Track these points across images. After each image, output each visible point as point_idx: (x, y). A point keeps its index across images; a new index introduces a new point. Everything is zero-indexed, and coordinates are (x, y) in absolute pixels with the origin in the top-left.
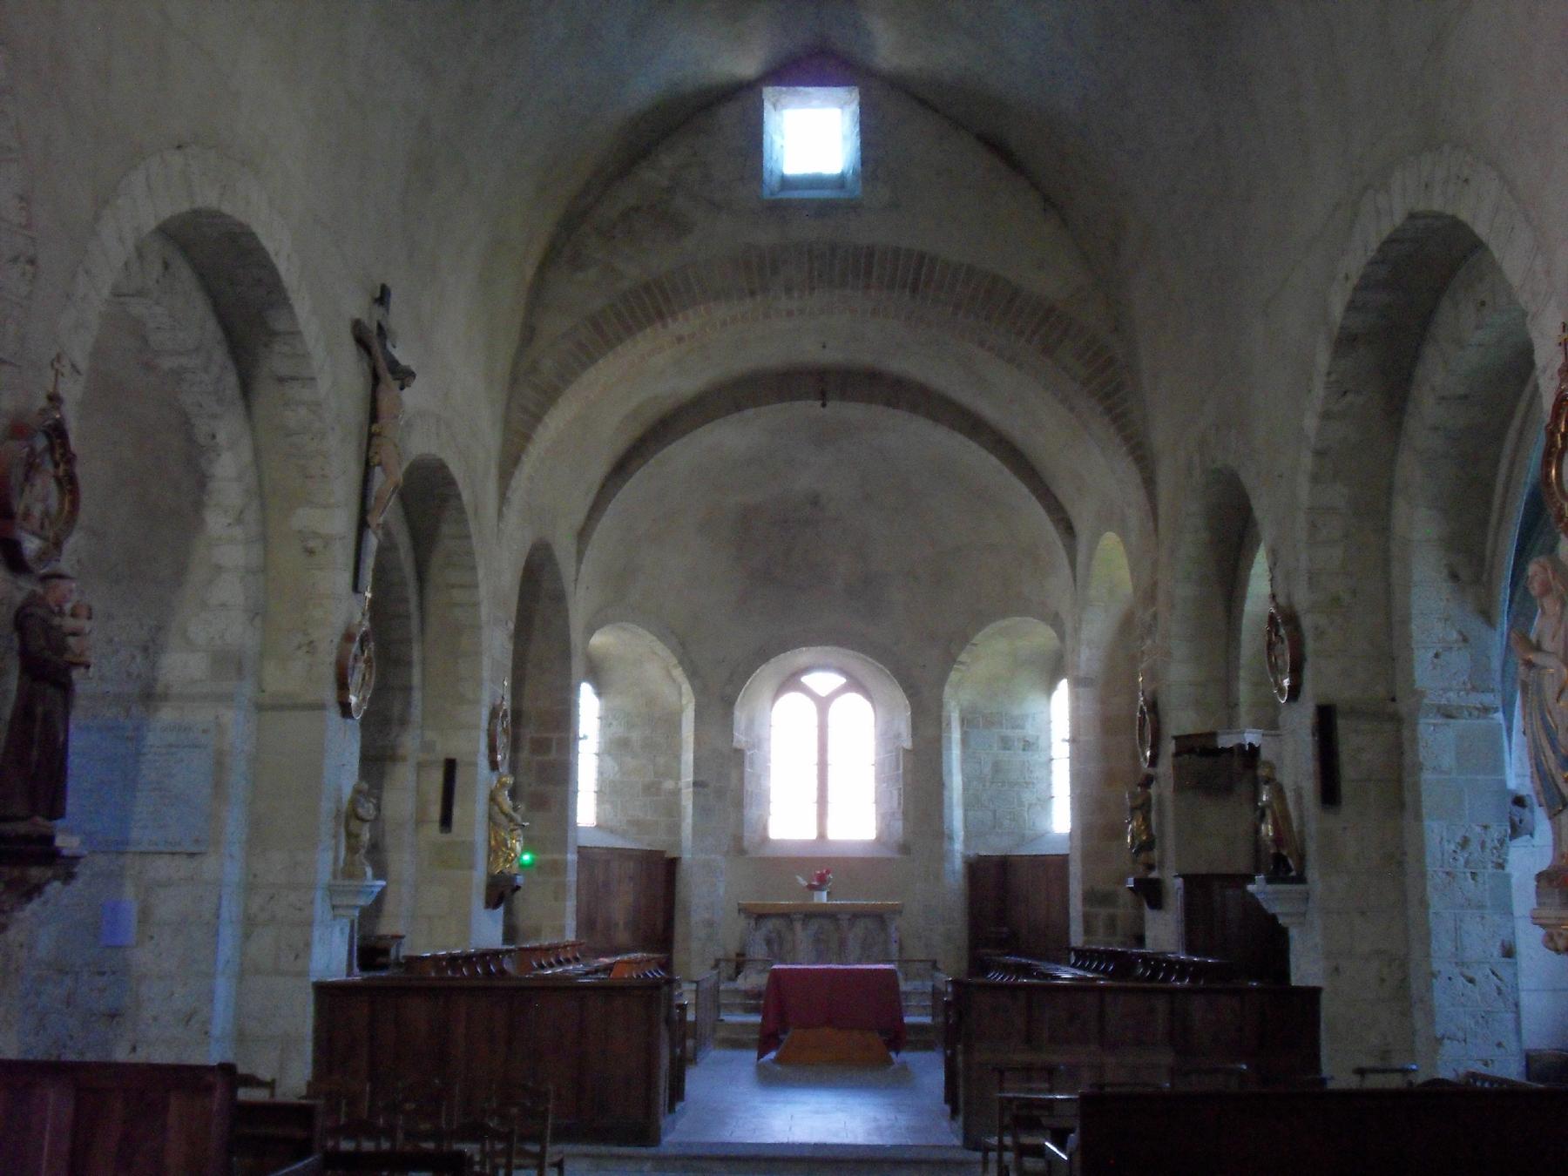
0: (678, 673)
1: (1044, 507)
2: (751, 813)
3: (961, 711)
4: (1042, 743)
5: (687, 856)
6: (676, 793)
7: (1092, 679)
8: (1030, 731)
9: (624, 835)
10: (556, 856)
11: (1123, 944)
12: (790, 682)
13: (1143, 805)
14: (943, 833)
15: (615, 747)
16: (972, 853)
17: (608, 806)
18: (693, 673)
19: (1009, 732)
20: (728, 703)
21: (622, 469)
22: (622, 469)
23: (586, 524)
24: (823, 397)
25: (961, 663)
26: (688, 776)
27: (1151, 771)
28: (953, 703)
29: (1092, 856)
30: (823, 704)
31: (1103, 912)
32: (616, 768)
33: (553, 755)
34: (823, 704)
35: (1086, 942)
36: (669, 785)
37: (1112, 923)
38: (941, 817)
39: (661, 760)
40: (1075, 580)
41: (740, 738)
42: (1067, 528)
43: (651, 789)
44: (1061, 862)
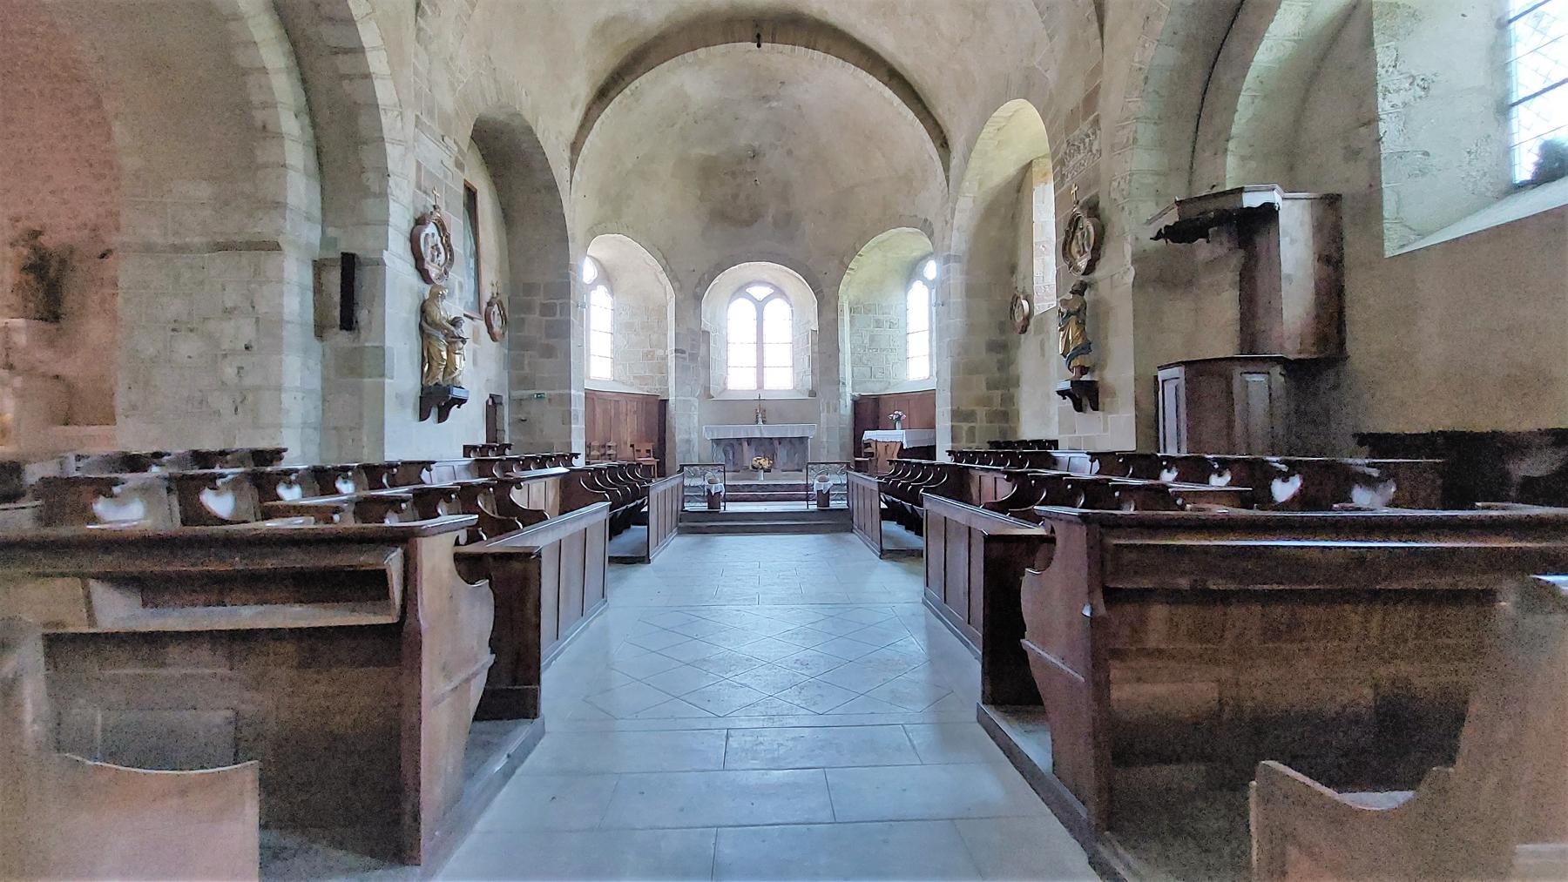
0: (663, 277)
2: (715, 373)
5: (672, 399)
6: (665, 358)
9: (632, 385)
12: (741, 290)
13: (1079, 310)
15: (622, 328)
18: (673, 278)
21: (603, 95)
22: (603, 95)
23: (576, 138)
24: (758, 40)
26: (672, 347)
27: (1085, 279)
28: (845, 297)
30: (760, 305)
31: (965, 426)
33: (558, 316)
34: (760, 305)
36: (660, 352)
37: (971, 431)
41: (706, 323)
43: (648, 355)
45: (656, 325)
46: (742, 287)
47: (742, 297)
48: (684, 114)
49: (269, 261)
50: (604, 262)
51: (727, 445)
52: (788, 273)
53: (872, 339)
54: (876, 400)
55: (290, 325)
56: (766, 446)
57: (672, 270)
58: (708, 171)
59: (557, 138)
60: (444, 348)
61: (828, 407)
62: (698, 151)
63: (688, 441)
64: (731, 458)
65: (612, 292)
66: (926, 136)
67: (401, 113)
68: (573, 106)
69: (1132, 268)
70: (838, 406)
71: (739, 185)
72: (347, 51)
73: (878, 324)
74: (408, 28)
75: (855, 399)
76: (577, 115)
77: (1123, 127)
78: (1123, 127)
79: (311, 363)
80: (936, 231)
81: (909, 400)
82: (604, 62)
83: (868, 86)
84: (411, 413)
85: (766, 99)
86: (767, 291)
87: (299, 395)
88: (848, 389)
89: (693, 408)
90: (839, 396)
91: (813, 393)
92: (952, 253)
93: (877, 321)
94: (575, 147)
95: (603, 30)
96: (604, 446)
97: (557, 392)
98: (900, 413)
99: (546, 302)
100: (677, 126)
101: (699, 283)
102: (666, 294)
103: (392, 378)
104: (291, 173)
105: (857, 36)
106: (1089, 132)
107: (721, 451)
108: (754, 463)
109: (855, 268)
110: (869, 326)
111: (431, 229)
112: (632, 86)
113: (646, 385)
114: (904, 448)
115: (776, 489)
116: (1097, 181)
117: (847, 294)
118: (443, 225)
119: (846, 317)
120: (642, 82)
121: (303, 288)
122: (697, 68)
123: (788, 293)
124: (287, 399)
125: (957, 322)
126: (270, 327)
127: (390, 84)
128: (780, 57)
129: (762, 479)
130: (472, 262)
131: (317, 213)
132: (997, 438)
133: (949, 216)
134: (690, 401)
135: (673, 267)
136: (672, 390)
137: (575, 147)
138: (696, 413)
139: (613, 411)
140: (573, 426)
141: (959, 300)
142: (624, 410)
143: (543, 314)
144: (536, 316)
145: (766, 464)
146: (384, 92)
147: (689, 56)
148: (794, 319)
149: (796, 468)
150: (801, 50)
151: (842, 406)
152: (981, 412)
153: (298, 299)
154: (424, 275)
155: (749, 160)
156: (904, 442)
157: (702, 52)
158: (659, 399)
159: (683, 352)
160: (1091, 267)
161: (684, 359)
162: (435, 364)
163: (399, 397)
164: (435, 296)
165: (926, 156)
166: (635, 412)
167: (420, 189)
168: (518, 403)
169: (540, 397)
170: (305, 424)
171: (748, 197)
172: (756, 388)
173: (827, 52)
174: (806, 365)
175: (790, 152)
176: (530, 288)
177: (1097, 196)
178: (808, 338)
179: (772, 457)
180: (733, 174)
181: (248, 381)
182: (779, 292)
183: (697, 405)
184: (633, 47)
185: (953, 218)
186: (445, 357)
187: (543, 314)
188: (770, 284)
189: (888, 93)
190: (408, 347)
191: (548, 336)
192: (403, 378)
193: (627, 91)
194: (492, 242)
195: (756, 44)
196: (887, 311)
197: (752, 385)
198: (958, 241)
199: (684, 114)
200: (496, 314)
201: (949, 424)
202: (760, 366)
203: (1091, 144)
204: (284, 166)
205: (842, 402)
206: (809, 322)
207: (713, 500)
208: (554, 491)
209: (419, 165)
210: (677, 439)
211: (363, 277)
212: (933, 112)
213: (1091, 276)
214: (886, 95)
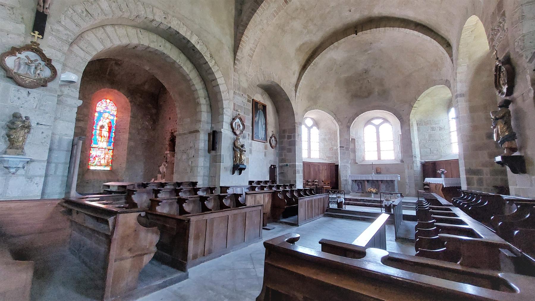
1: (439, 43)
2: (358, 154)
3: (417, 121)
5: (339, 164)
6: (337, 150)
7: (464, 94)
8: (441, 124)
9: (325, 160)
11: (486, 189)
12: (368, 122)
16: (423, 161)
17: (322, 154)
18: (338, 121)
19: (434, 126)
20: (349, 127)
21: (304, 68)
22: (304, 68)
25: (415, 107)
26: (339, 146)
28: (414, 119)
29: (466, 157)
30: (377, 127)
31: (475, 177)
33: (292, 139)
34: (377, 127)
35: (468, 188)
36: (335, 148)
39: (333, 142)
40: (453, 63)
42: (447, 45)
43: (331, 149)
44: (456, 162)
45: (333, 138)
46: (369, 120)
47: (370, 124)
48: (336, 65)
49: (198, 134)
50: (315, 119)
51: (358, 182)
52: (387, 113)
53: (430, 136)
55: (201, 151)
56: (375, 183)
57: (338, 118)
58: (348, 82)
59: (289, 85)
60: (239, 154)
61: (408, 167)
62: (344, 76)
63: (346, 180)
64: (361, 188)
65: (318, 128)
66: (438, 45)
67: (228, 92)
68: (294, 74)
69: (532, 88)
70: (413, 167)
71: (362, 84)
72: (213, 80)
73: (433, 129)
74: (231, 69)
75: (423, 163)
76: (297, 75)
77: (516, 12)
78: (516, 12)
79: (207, 160)
80: (451, 85)
81: (450, 164)
82: (302, 58)
83: (407, 33)
84: (229, 173)
85: (366, 51)
86: (380, 121)
87: (203, 168)
89: (348, 168)
91: (402, 161)
92: (458, 93)
94: (296, 86)
95: (299, 49)
96: (314, 181)
98: (443, 170)
99: (289, 135)
100: (334, 70)
102: (336, 127)
103: (223, 163)
104: (203, 113)
105: (396, 16)
106: (500, 20)
107: (357, 184)
109: (417, 106)
110: (428, 130)
111: (237, 120)
112: (313, 62)
113: (330, 159)
114: (444, 187)
115: (375, 202)
116: (508, 45)
117: (414, 118)
118: (241, 119)
120: (316, 60)
121: (205, 141)
122: (336, 49)
123: (389, 120)
124: (199, 169)
125: (466, 125)
126: (197, 150)
127: (225, 85)
128: (366, 35)
129: (373, 198)
130: (264, 127)
131: (210, 121)
133: (455, 77)
134: (347, 165)
135: (338, 117)
136: (339, 161)
137: (296, 86)
139: (317, 169)
140: (297, 175)
141: (465, 115)
142: (321, 169)
143: (288, 139)
144: (286, 140)
145: (374, 191)
146: (222, 88)
147: (332, 46)
150: (374, 30)
153: (204, 144)
154: (235, 133)
155: (364, 74)
157: (336, 44)
158: (335, 164)
160: (510, 91)
161: (344, 149)
162: (236, 158)
163: (226, 169)
164: (237, 139)
165: (441, 53)
166: (326, 170)
167: (235, 110)
168: (281, 167)
169: (287, 165)
170: (204, 176)
171: (366, 87)
172: (377, 159)
173: (385, 27)
174: (398, 149)
175: (381, 67)
176: (284, 131)
177: (509, 52)
178: (399, 138)
179: (378, 188)
180: (359, 81)
181: (193, 165)
182: (386, 120)
183: (350, 166)
184: (312, 50)
185: (456, 77)
186: (239, 156)
187: (288, 139)
188: (382, 118)
189: (416, 33)
190: (229, 154)
191: (290, 145)
192: (227, 161)
193: (312, 64)
194: (272, 119)
195: (355, 34)
197: (376, 158)
198: (461, 86)
199: (336, 65)
200: (273, 140)
201: (465, 176)
202: (379, 150)
203: (504, 26)
204: (201, 111)
205: (415, 165)
206: (398, 131)
207: (340, 205)
208: (268, 197)
209: (234, 104)
210: (342, 179)
211: (218, 136)
212: (440, 34)
213: (512, 96)
214: (416, 34)
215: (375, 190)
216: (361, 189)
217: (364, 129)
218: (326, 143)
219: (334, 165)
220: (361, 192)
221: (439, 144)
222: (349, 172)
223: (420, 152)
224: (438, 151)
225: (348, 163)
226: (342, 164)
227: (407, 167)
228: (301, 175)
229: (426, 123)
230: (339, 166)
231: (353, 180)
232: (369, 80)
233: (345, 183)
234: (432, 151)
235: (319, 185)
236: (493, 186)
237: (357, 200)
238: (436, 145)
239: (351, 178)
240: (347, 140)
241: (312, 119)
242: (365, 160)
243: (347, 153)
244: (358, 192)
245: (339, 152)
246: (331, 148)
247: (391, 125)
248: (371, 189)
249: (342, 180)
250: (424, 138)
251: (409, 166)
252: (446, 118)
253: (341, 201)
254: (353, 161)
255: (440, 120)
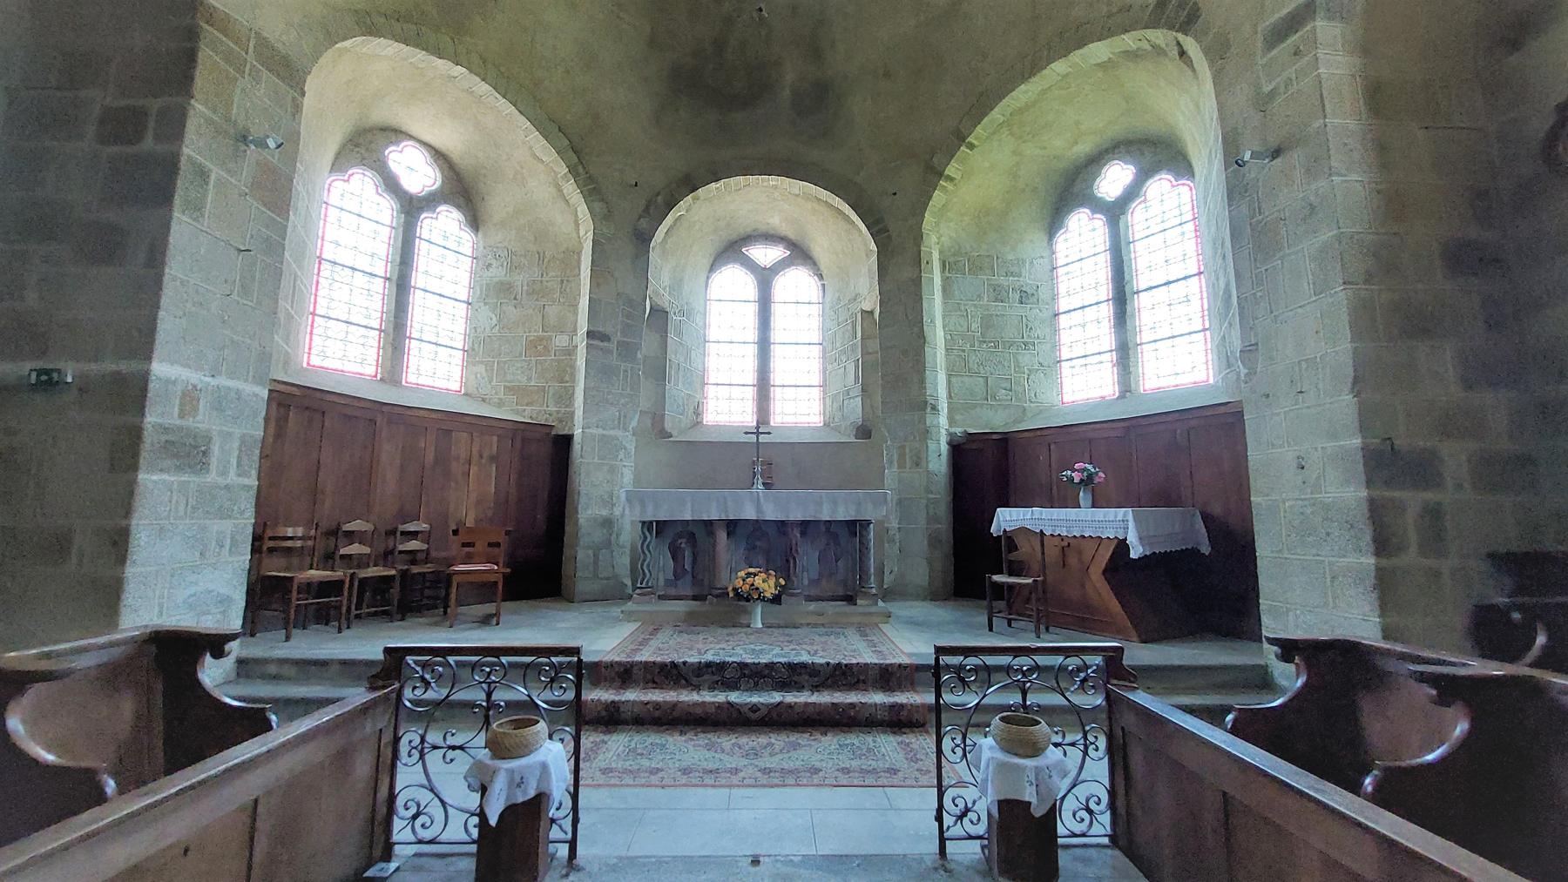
0: (571, 188)
2: (676, 390)
4: (1044, 294)
5: (578, 432)
6: (570, 351)
8: (1027, 279)
9: (500, 404)
10: (124, 367)
12: (732, 249)
14: (926, 402)
16: (958, 430)
17: (481, 369)
18: (592, 189)
19: (1002, 280)
20: (643, 239)
25: (950, 179)
26: (583, 327)
28: (934, 239)
30: (765, 278)
31: (1413, 500)
32: (494, 321)
33: (148, 144)
34: (765, 278)
36: (561, 341)
38: (922, 381)
43: (537, 346)
53: (987, 322)
54: (1003, 444)
61: (902, 456)
65: (475, 221)
73: (999, 294)
75: (114, 771)
88: (943, 420)
89: (621, 456)
90: (926, 433)
91: (864, 432)
93: (996, 288)
96: (392, 532)
97: (109, 366)
101: (647, 210)
102: (577, 225)
108: (739, 583)
109: (957, 176)
110: (980, 297)
119: (935, 278)
132: (1511, 540)
136: (579, 413)
138: (629, 463)
145: (768, 586)
148: (828, 299)
149: (841, 592)
151: (932, 456)
152: (1455, 458)
156: (1132, 539)
159: (605, 338)
161: (609, 352)
166: (493, 459)
169: (48, 382)
178: (854, 328)
182: (800, 253)
183: (631, 447)
196: (1015, 269)
205: (932, 446)
215: (772, 582)
216: (689, 578)
217: (708, 278)
218: (509, 309)
219: (548, 434)
220: (689, 592)
221: (1017, 361)
222: (628, 477)
223: (949, 388)
224: (1011, 390)
225: (626, 430)
226: (594, 431)
227: (895, 457)
228: (232, 477)
229: (977, 267)
230: (577, 439)
231: (651, 522)
232: (762, 6)
233: (598, 535)
234: (991, 389)
235: (434, 554)
236: (1492, 556)
237: (669, 674)
238: (1006, 364)
239: (638, 508)
240: (630, 302)
241: (440, 156)
242: (701, 422)
243: (626, 371)
244: (673, 592)
245: (581, 362)
246: (541, 339)
247: (821, 277)
248: (749, 575)
249: (581, 521)
250: (966, 327)
251: (907, 450)
252: (1044, 255)
253: (532, 793)
254: (649, 422)
255: (1024, 261)
